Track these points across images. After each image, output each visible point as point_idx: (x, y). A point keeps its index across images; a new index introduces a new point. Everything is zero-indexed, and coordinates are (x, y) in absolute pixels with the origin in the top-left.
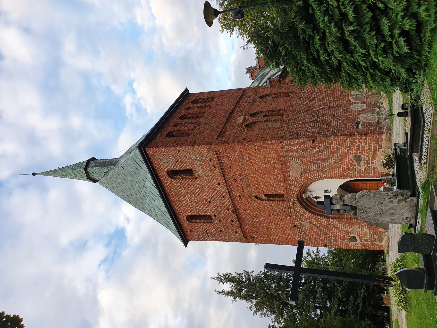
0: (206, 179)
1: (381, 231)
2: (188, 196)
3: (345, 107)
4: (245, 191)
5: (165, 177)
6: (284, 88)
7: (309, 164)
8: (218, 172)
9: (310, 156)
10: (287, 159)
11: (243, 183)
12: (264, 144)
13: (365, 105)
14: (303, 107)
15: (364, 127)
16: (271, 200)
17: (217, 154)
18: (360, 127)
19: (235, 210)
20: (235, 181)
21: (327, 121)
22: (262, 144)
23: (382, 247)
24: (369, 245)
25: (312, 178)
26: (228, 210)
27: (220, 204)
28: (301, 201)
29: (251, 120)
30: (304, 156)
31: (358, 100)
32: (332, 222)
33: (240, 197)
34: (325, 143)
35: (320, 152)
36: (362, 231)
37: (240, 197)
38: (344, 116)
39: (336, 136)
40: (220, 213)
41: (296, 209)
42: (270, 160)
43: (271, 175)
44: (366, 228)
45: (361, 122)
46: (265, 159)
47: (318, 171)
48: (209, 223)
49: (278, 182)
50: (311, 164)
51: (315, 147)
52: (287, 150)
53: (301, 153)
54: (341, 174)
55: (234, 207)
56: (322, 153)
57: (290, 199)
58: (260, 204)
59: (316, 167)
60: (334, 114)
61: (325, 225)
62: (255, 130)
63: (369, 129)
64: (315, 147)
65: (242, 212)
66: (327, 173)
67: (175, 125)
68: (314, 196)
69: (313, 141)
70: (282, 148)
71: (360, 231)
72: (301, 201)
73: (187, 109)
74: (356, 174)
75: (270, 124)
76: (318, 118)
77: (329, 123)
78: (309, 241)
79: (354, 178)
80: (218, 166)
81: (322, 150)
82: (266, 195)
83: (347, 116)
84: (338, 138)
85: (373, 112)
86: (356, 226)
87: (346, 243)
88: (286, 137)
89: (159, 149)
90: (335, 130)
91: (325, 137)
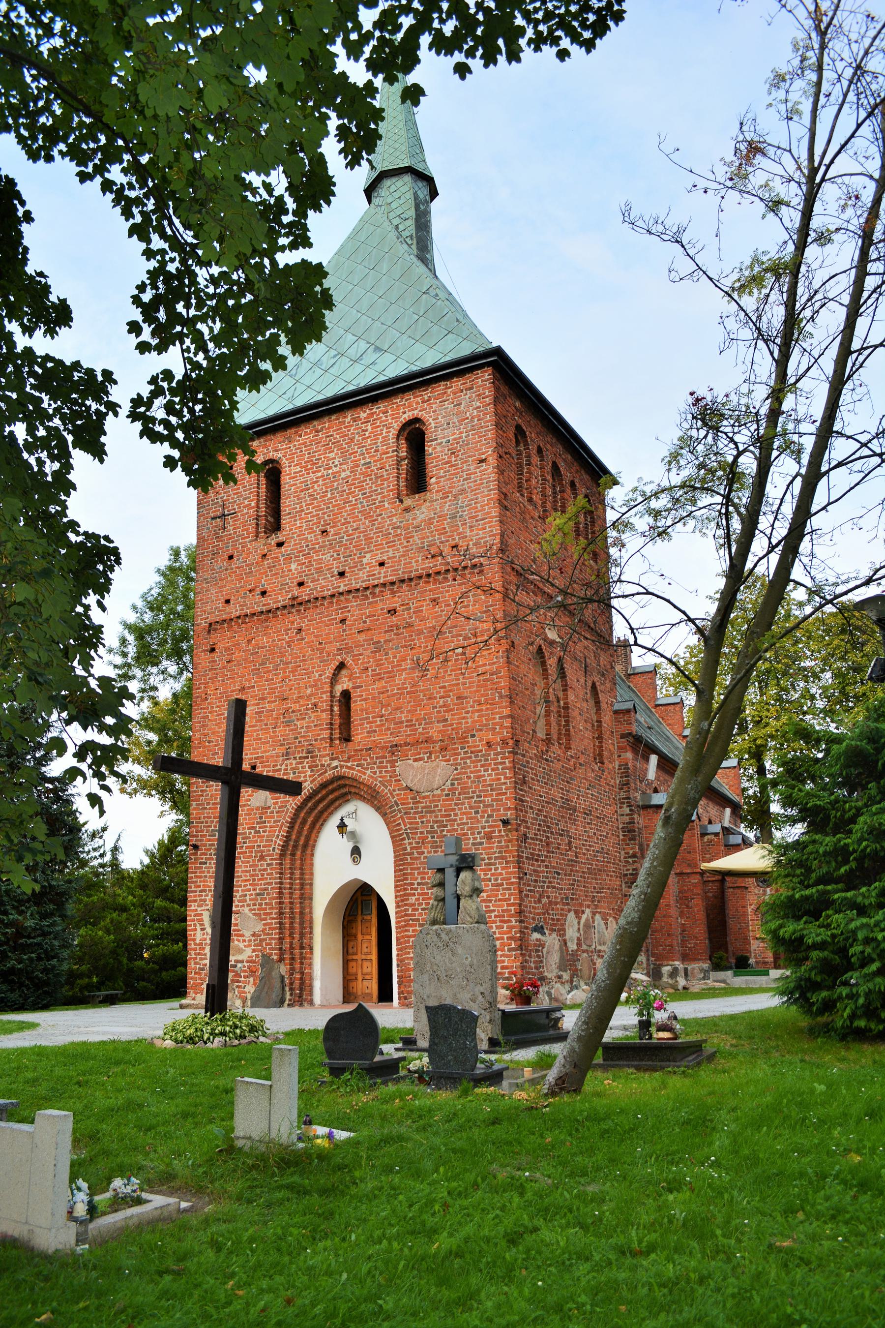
0: (398, 527)
1: (246, 990)
2: (344, 470)
3: (572, 899)
4: (362, 637)
5: (404, 413)
6: (611, 747)
7: (440, 811)
8: (419, 565)
9: (464, 813)
10: (456, 754)
11: (386, 632)
12: (501, 697)
13: (575, 947)
14: (573, 795)
15: (535, 945)
16: (332, 706)
17: (474, 566)
18: (536, 936)
19: (301, 604)
20: (393, 612)
21: (546, 857)
22: (500, 693)
23: (196, 993)
24: (201, 959)
25: (401, 817)
26: (301, 584)
27: (319, 562)
28: (331, 787)
29: (552, 662)
30: (465, 798)
31: (585, 932)
32: (268, 865)
33: (343, 621)
34: (500, 852)
35: (475, 839)
36: (244, 941)
37: (343, 621)
38: (556, 897)
39: (520, 878)
40: (288, 560)
41: (309, 773)
42: (452, 710)
43: (409, 712)
44: (254, 951)
45: (543, 938)
46: (458, 698)
47: (422, 833)
48: (257, 524)
49: (389, 729)
50: (442, 816)
51: (489, 827)
52: (483, 756)
53: (473, 792)
54: (412, 889)
55: (309, 601)
56: (473, 844)
57: (337, 758)
58: (320, 675)
59: (432, 827)
60: (559, 874)
61: (259, 846)
62: (530, 672)
63: (530, 956)
64: (489, 827)
65: (292, 623)
66: (416, 855)
67: (540, 451)
68: (346, 821)
69: (505, 822)
70: (489, 744)
71: (242, 935)
72: (331, 787)
73: (573, 484)
74: (411, 926)
75: (540, 710)
76: (552, 833)
77: (543, 861)
78: (208, 804)
79: (397, 923)
80: (435, 566)
81: (482, 843)
82: (346, 695)
83: (556, 903)
84: (512, 883)
85: (562, 967)
86: (259, 927)
87: (205, 901)
88: (517, 753)
89: (489, 404)
90: (531, 875)
91: (518, 851)
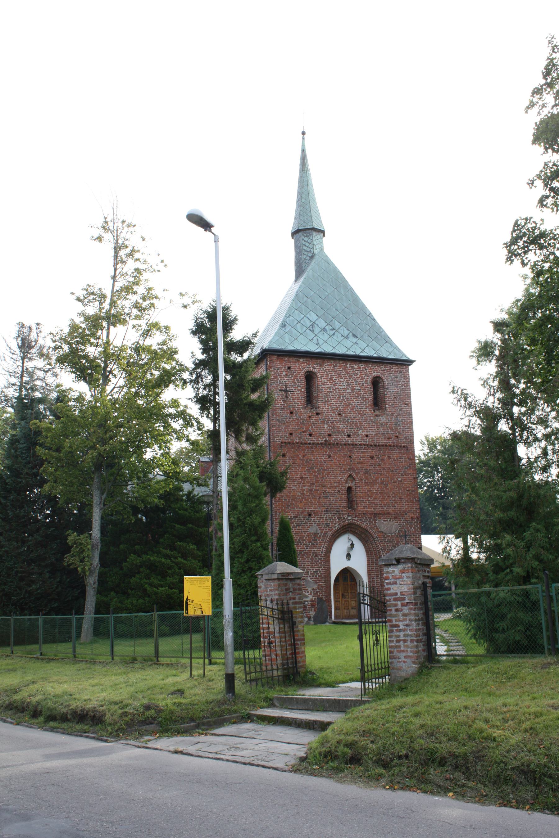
4: (359, 466)
17: (404, 447)
27: (338, 427)
55: (334, 444)
70: (412, 518)
